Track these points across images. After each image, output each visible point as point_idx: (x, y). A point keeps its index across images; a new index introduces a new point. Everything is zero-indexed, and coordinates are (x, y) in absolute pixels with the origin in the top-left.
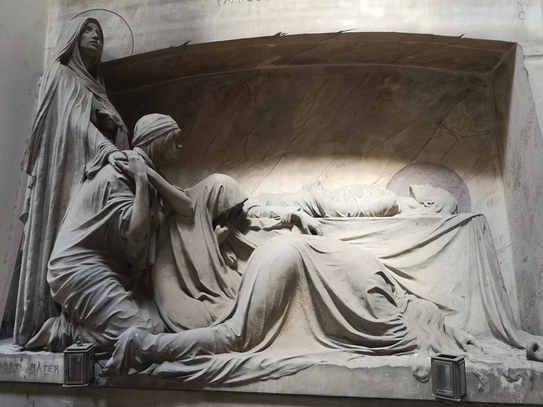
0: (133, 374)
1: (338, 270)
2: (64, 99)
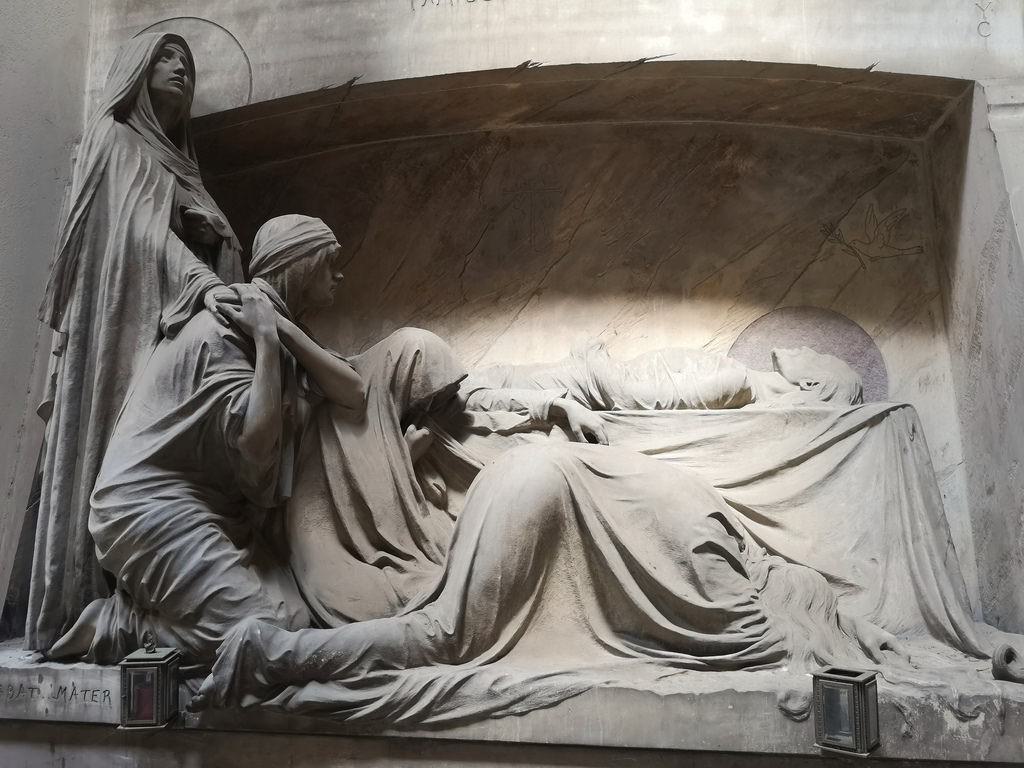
0: (251, 706)
1: (637, 510)
2: (122, 188)
